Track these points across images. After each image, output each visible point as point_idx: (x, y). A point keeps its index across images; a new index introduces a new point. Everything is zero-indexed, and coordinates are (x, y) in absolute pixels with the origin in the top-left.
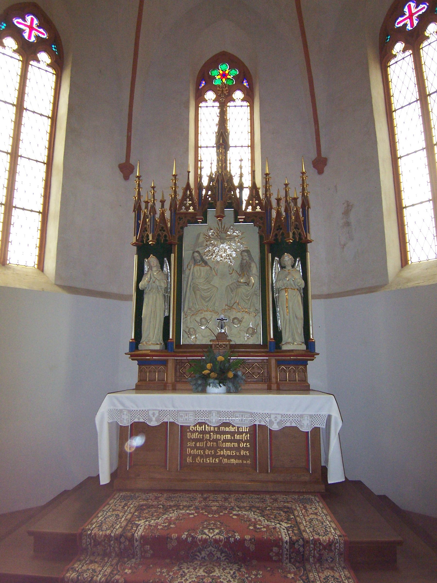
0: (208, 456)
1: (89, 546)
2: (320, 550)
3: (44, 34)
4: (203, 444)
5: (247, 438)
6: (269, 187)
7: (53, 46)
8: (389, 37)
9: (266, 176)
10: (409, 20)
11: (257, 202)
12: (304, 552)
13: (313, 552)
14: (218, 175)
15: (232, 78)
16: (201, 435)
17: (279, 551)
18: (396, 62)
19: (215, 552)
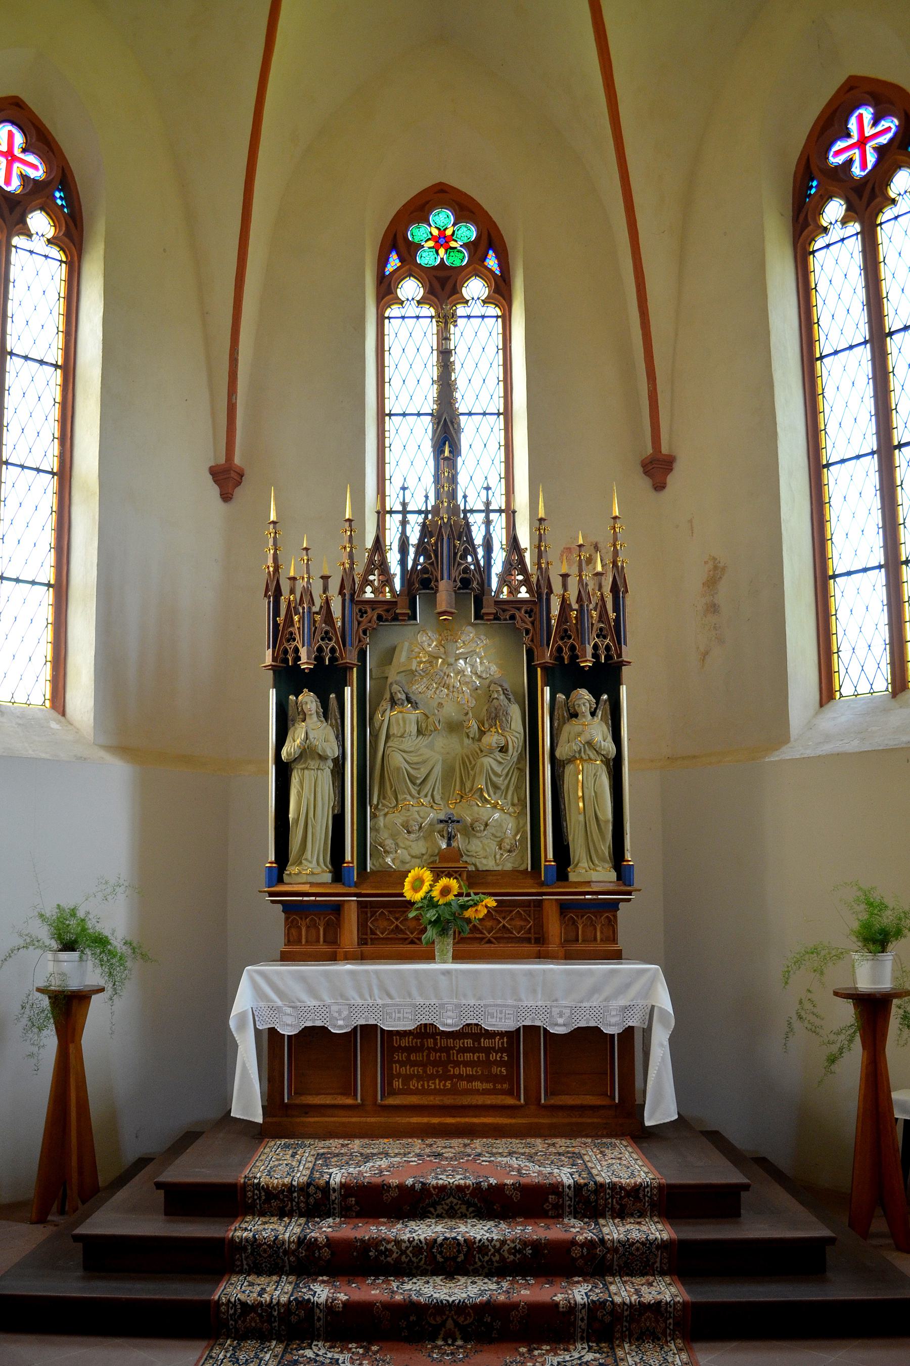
0: (432, 1077)
1: (258, 1201)
2: (621, 1197)
3: (35, 168)
4: (423, 1056)
5: (502, 1043)
6: (546, 546)
7: (57, 194)
8: (815, 183)
9: (538, 524)
10: (857, 151)
11: (520, 578)
12: (596, 1201)
13: (610, 1200)
14: (441, 526)
15: (461, 246)
16: (419, 1041)
17: (559, 1201)
18: (828, 246)
19: (458, 1206)
